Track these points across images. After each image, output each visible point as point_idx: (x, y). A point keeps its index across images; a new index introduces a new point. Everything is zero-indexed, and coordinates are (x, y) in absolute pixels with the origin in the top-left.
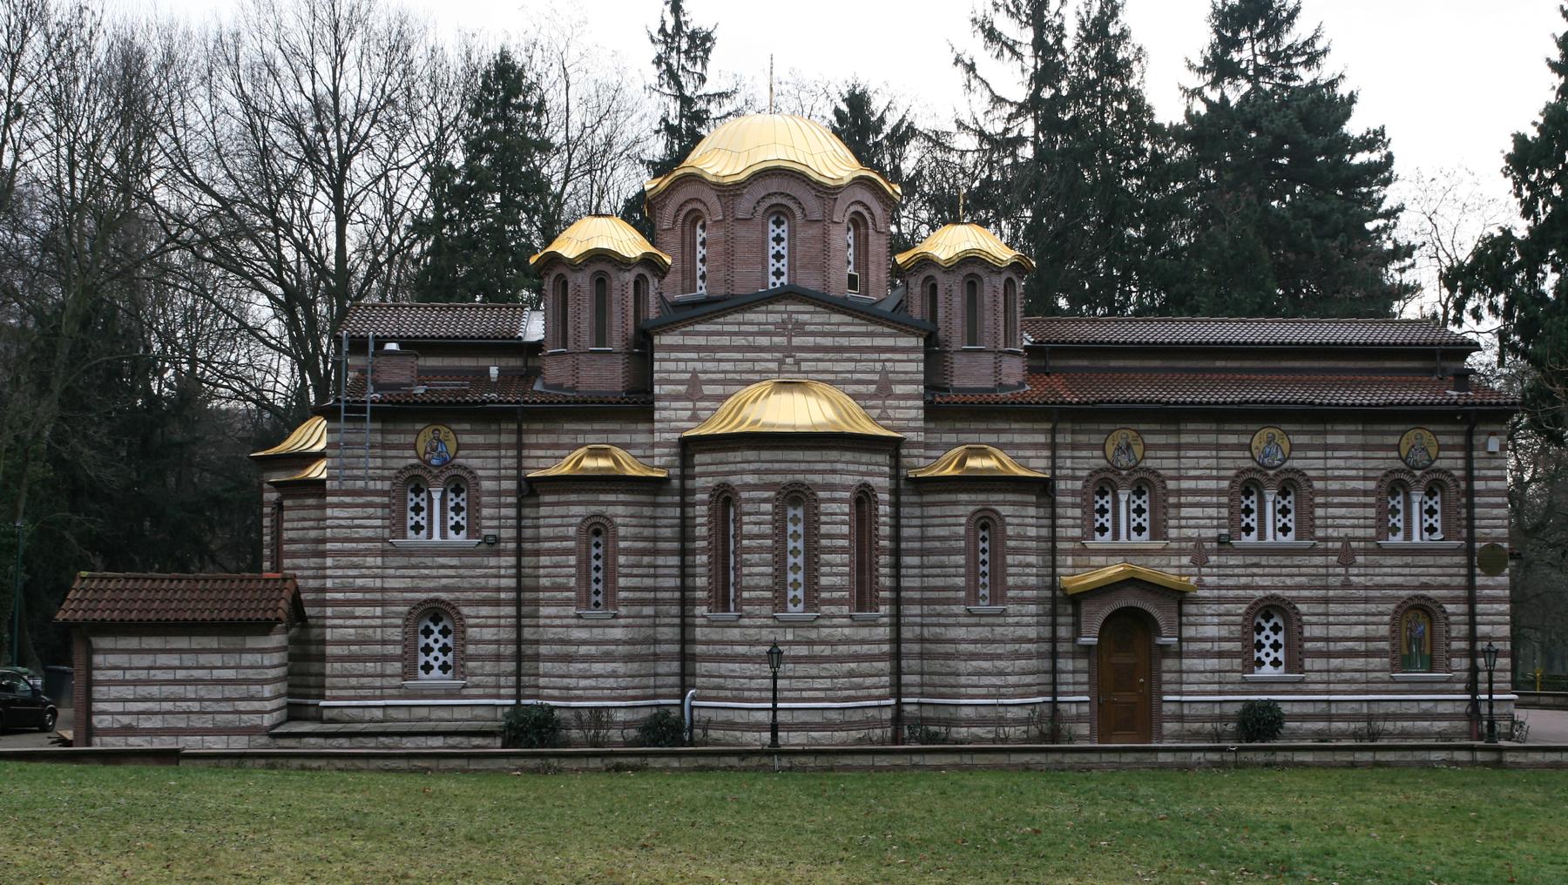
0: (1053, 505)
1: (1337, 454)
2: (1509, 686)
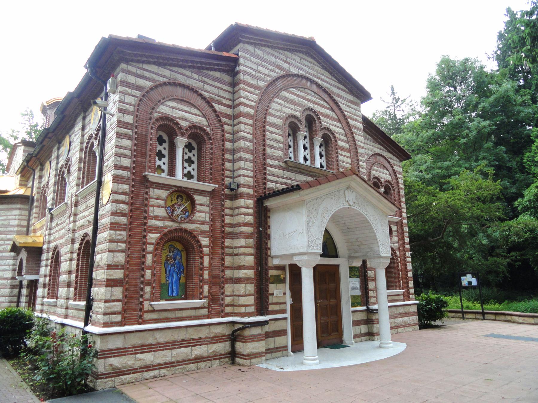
0: (30, 210)
2: (402, 297)
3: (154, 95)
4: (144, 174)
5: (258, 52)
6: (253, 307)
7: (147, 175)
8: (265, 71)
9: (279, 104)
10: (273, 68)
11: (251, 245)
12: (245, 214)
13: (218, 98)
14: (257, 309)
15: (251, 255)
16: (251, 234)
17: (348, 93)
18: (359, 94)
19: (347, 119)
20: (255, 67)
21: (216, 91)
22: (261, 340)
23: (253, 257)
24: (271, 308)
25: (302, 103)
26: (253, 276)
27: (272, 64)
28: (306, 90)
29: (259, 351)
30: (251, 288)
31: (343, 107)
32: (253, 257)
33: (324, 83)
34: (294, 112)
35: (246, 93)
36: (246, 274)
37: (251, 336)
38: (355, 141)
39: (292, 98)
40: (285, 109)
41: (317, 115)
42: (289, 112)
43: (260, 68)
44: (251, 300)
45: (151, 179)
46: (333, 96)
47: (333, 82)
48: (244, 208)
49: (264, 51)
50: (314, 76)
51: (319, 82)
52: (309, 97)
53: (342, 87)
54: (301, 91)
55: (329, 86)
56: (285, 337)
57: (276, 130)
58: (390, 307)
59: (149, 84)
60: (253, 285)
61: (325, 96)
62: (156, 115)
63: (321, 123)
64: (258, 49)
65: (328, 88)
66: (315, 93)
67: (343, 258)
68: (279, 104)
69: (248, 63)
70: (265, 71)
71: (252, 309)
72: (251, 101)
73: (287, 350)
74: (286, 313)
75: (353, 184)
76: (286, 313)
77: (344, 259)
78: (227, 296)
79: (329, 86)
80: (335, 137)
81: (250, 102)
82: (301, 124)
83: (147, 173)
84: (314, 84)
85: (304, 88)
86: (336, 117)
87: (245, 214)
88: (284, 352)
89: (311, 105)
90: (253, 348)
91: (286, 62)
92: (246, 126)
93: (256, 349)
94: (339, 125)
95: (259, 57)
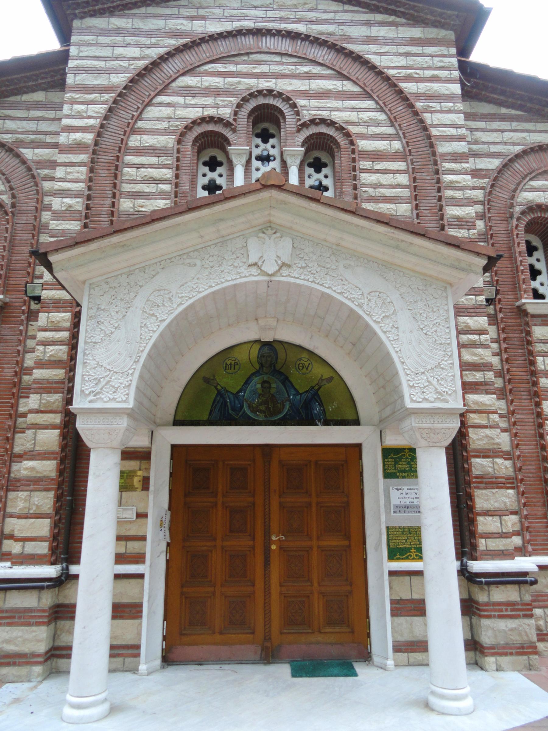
1: (379, 166)
3: (508, 177)
4: (517, 304)
5: (117, 22)
6: (46, 544)
7: (524, 304)
8: (135, 52)
9: (169, 105)
10: (154, 40)
11: (54, 407)
12: (45, 343)
13: (32, 137)
14: (53, 550)
15: (53, 427)
16: (56, 383)
17: (402, 25)
18: (441, 15)
19: (395, 85)
20: (107, 52)
21: (32, 126)
22: (38, 624)
23: (56, 432)
24: (482, 544)
25: (240, 87)
26: (54, 475)
27: (149, 34)
28: (252, 56)
29: (25, 648)
30: (45, 501)
31: (375, 60)
32: (57, 432)
33: (314, 27)
34: (210, 112)
35: (76, 106)
36: (32, 469)
37: (7, 611)
38: (425, 129)
39: (207, 84)
40: (181, 112)
41: (288, 99)
42: (195, 113)
43: (119, 51)
44: (43, 527)
45: (531, 310)
46: (345, 45)
47: (347, 17)
48: (46, 330)
49: (128, 16)
50: (283, 20)
51: (301, 28)
52: (264, 68)
53: (379, 17)
54: (237, 63)
55: (331, 28)
56: (136, 621)
57: (153, 160)
58: (117, 577)
59: (494, 163)
60: (52, 494)
61: (320, 54)
62: (518, 209)
63: (298, 113)
64: (120, 16)
65: (322, 34)
66: (282, 54)
67: (365, 425)
68: (169, 105)
69: (86, 51)
70: (135, 52)
71: (43, 548)
72: (89, 117)
73: (138, 655)
74: (143, 562)
75: (280, 217)
76: (143, 562)
77: (371, 428)
78: (11, 516)
79: (331, 28)
80: (348, 135)
81: (87, 121)
82: (234, 131)
83: (523, 301)
84: (283, 36)
85: (248, 54)
86: (356, 89)
87: (45, 343)
88: (128, 660)
89: (267, 84)
90: (8, 642)
91: (193, 18)
92: (69, 169)
93: (16, 645)
94: (370, 104)
95: (118, 32)
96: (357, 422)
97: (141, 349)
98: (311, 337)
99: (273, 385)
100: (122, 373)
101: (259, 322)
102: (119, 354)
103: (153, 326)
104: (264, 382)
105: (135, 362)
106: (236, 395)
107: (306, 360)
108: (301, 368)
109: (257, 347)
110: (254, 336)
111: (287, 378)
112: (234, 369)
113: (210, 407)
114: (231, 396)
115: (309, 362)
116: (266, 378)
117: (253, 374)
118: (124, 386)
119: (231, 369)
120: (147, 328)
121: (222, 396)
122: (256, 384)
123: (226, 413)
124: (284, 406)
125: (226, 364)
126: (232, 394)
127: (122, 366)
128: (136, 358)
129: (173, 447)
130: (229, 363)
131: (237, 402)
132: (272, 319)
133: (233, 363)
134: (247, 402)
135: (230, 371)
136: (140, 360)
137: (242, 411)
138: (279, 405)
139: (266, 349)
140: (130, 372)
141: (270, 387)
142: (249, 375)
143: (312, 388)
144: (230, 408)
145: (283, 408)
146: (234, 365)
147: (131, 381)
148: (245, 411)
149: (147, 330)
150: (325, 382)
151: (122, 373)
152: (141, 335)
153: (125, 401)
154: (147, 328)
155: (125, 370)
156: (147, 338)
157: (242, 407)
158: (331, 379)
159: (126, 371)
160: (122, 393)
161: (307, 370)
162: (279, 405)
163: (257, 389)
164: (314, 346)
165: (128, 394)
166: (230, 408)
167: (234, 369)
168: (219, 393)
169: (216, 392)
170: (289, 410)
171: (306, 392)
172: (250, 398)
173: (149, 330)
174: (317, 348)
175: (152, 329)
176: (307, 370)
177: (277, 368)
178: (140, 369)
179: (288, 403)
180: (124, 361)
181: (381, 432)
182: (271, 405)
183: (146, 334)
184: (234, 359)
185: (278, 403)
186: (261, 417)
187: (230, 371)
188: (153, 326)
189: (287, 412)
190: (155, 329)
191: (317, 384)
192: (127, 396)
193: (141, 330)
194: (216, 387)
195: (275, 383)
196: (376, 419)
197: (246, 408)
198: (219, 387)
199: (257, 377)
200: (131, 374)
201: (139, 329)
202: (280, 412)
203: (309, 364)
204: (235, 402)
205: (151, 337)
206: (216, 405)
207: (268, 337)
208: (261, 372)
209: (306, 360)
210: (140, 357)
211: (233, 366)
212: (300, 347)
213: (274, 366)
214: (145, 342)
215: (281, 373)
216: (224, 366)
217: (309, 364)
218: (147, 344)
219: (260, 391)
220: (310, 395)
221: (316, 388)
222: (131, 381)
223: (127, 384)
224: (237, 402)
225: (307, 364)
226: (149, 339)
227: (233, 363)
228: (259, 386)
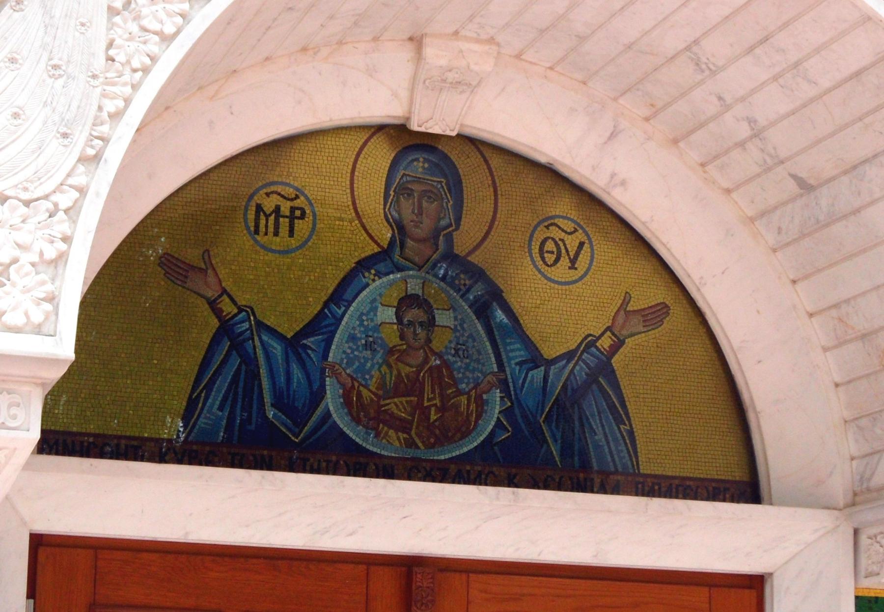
77: (822, 519)
96: (749, 490)
97: (110, 106)
98: (613, 136)
99: (443, 318)
100: (27, 203)
101: (429, 52)
102: (16, 116)
103: (162, 15)
104: (407, 301)
105: (83, 159)
106: (294, 344)
107: (569, 226)
108: (550, 258)
109: (380, 156)
110: (380, 105)
111: (496, 295)
112: (291, 233)
113: (186, 385)
114: (277, 349)
115: (580, 236)
116: (414, 287)
117: (364, 264)
118: (36, 258)
119: (276, 234)
120: (137, 18)
121: (238, 345)
122: (377, 304)
123: (255, 422)
124: (481, 404)
125: (259, 208)
126: (280, 337)
127: (28, 173)
128: (88, 144)
129: (39, 543)
130: (269, 205)
131: (297, 373)
132: (476, 47)
133: (285, 209)
134: (336, 375)
135: (276, 243)
136: (107, 154)
137: (319, 411)
138: (464, 399)
139: (419, 166)
140: (65, 200)
141: (430, 324)
142: (348, 265)
143: (590, 343)
144: (268, 398)
145: (479, 417)
146: (292, 218)
147: (66, 239)
148: (327, 415)
149: (134, 28)
150: (636, 323)
151: (27, 203)
152: (110, 45)
153: (38, 330)
154: (137, 18)
155: (39, 193)
156: (136, 64)
157: (318, 396)
158: (655, 315)
159: (46, 197)
160: (26, 290)
161: (573, 267)
162: (464, 399)
163: (377, 328)
164: (613, 175)
165: (51, 299)
166: (268, 398)
167: (291, 233)
168: (226, 328)
169: (215, 323)
170: (499, 424)
171: (569, 355)
172: (350, 363)
173: (145, 30)
174: (623, 183)
175: (156, 27)
176: (573, 267)
177: (460, 249)
178: (105, 191)
179: (498, 394)
180: (40, 148)
181: (856, 532)
182: (431, 398)
183: (133, 45)
184: (289, 192)
185: (459, 393)
186: (389, 446)
187: (276, 243)
188: (162, 15)
189: (492, 434)
190: (169, 29)
191: (608, 329)
192: (48, 307)
193: (111, 26)
194: (213, 304)
195: (452, 308)
196: (839, 486)
197: (332, 401)
198: (228, 308)
199: (379, 275)
200: (66, 211)
201: (102, 18)
202: (465, 432)
203: (582, 244)
204: (288, 374)
205: (153, 59)
206: (212, 381)
207: (436, 118)
208: (396, 257)
209: (569, 226)
210: (105, 140)
211: (284, 222)
212: (551, 174)
213: (449, 239)
214: (127, 77)
215: (478, 274)
216: (251, 215)
217: (582, 244)
218: (135, 87)
219: (391, 335)
220: (581, 372)
221: (605, 343)
222: (66, 239)
223: (51, 253)
224: (297, 373)
225: (572, 243)
226: (146, 70)
227: (285, 209)
228: (387, 314)
